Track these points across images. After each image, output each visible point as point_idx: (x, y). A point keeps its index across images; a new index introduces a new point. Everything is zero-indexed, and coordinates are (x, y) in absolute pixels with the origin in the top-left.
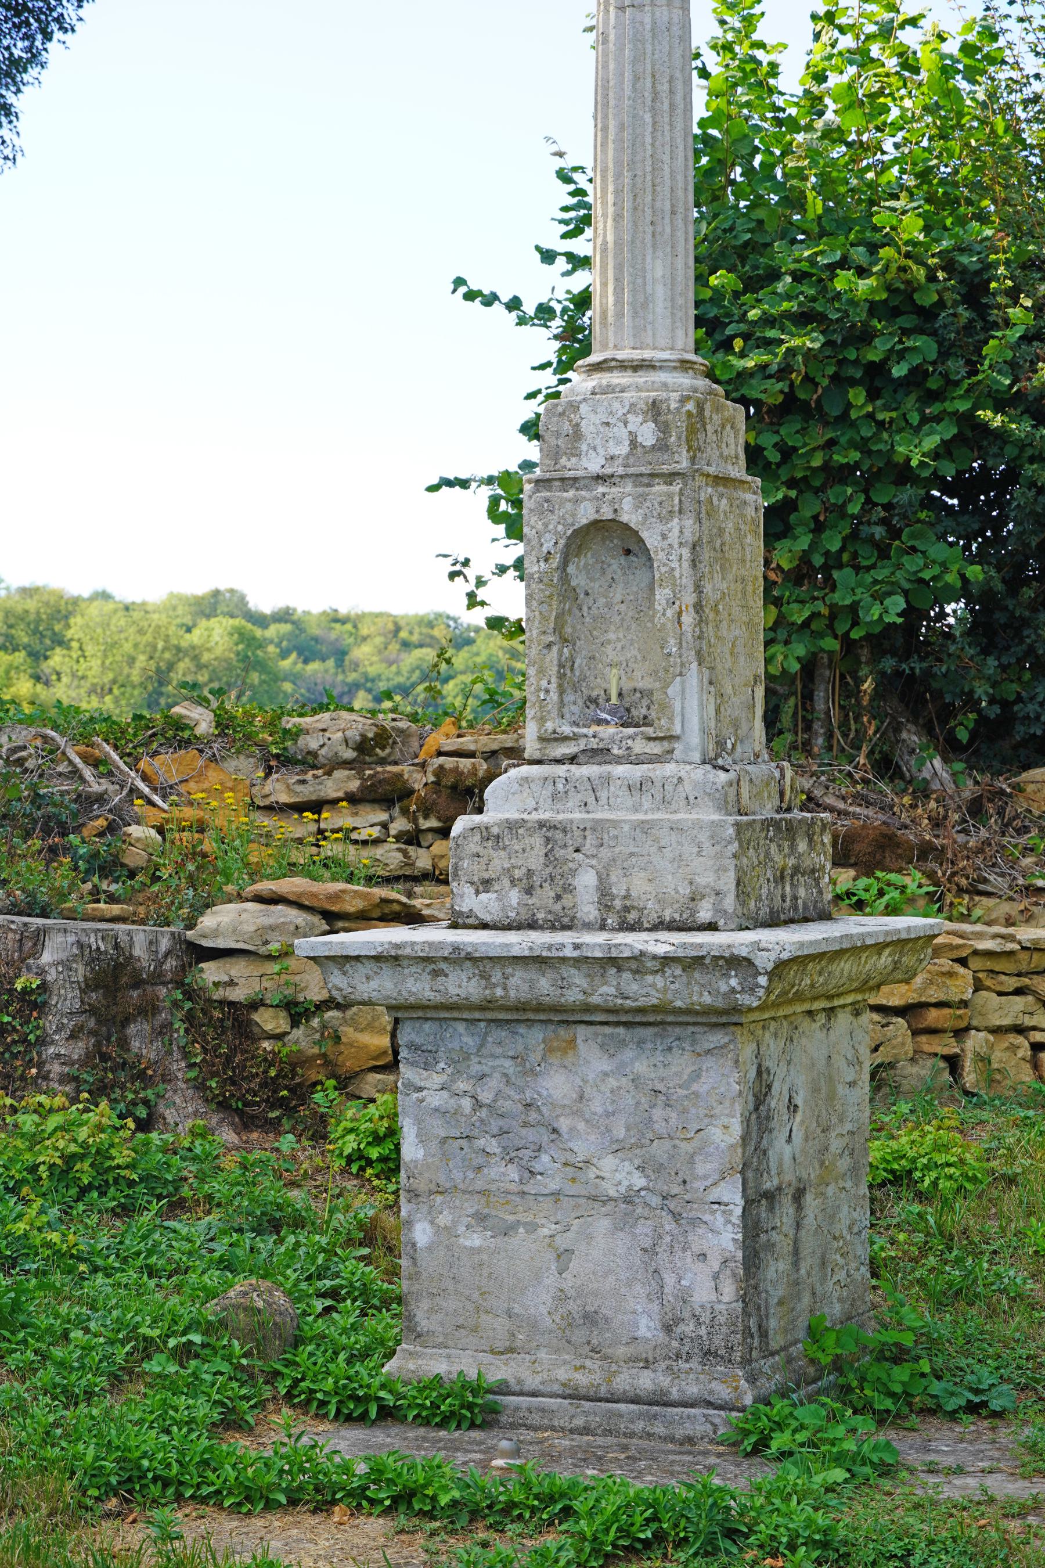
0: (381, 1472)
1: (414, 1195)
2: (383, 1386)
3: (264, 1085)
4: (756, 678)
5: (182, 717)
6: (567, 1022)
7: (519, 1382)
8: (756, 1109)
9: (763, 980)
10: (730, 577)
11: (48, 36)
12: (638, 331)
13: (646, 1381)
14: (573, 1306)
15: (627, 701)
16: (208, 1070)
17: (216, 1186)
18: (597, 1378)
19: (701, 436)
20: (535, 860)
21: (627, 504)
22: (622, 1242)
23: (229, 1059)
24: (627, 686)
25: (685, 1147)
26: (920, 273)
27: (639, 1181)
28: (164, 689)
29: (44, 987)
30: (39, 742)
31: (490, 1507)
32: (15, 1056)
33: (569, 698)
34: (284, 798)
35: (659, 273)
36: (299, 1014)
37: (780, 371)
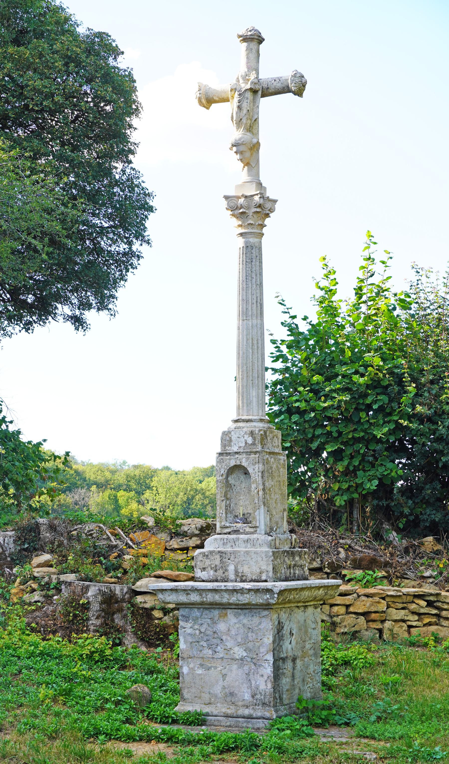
0: (165, 731)
1: (183, 658)
2: (173, 714)
3: (155, 633)
4: (284, 510)
5: (144, 520)
6: (225, 608)
7: (212, 712)
8: (278, 633)
9: (276, 596)
10: (275, 481)
11: (127, 270)
12: (248, 411)
13: (247, 712)
14: (227, 691)
15: (246, 517)
16: (137, 629)
17: (136, 662)
18: (233, 711)
19: (265, 441)
20: (217, 562)
21: (244, 460)
22: (240, 672)
23: (144, 625)
24: (246, 512)
26: (381, 375)
28: (190, 506)
29: (88, 603)
30: (97, 529)
31: (194, 741)
32: (80, 624)
33: (229, 515)
34: (176, 546)
35: (254, 394)
36: (166, 612)
37: (338, 407)
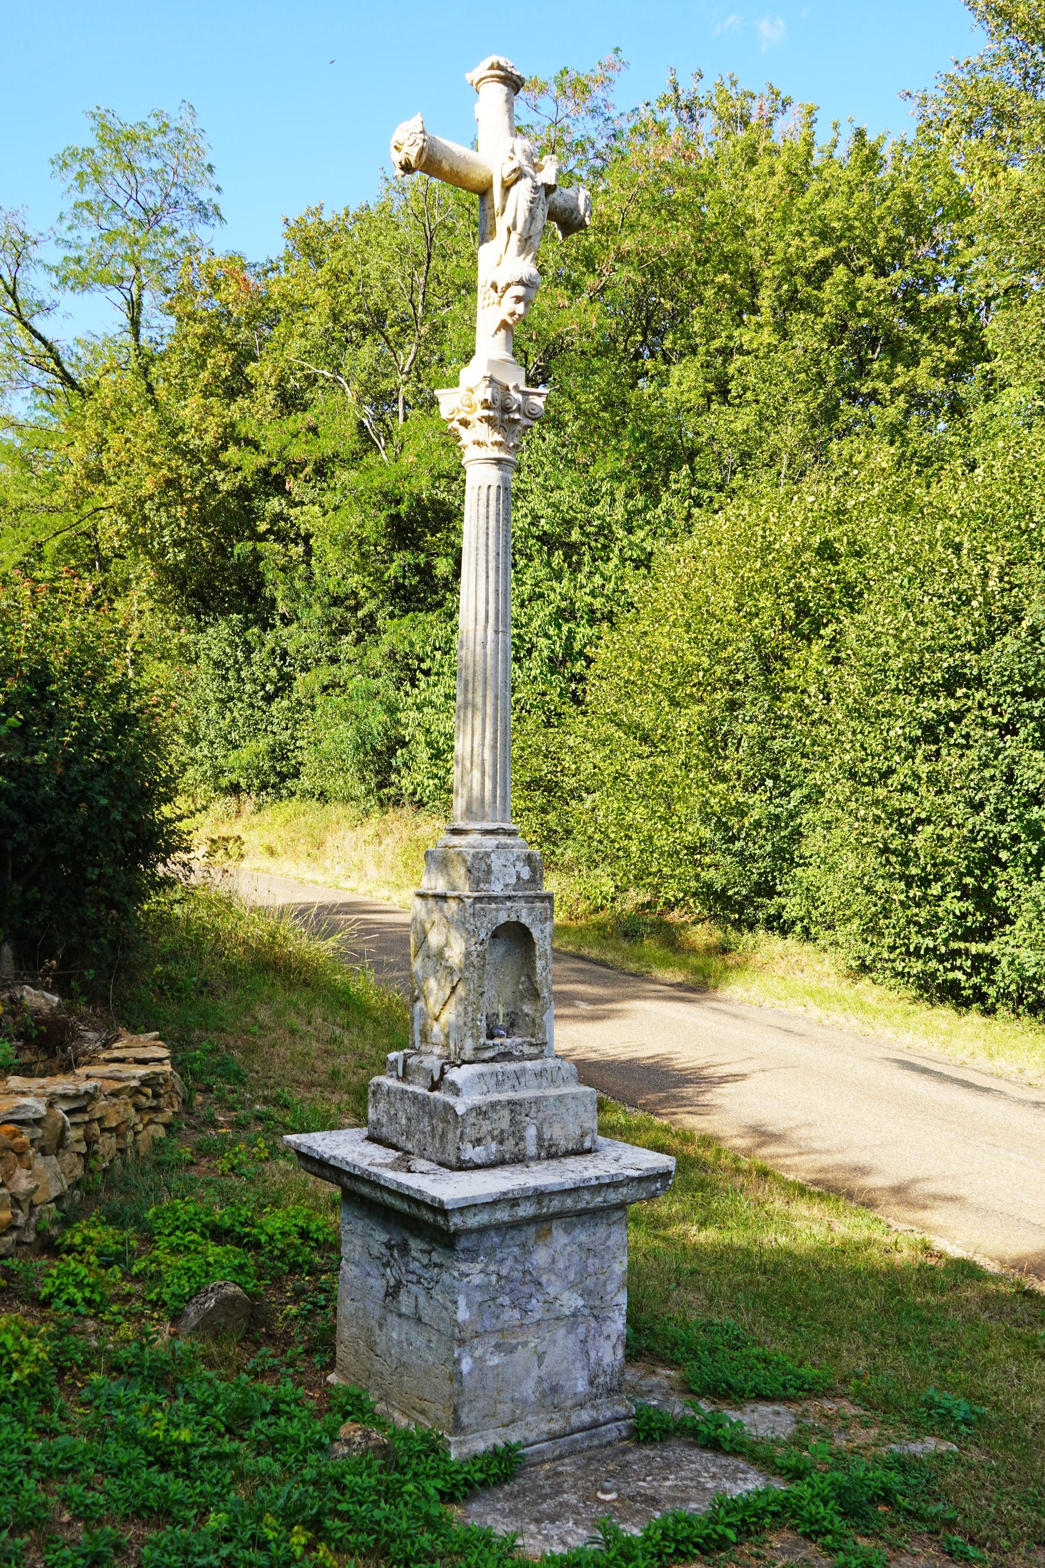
7: (526, 1439)
13: (585, 1416)
20: (505, 1124)
21: (524, 913)
25: (602, 1278)
27: (580, 1302)
